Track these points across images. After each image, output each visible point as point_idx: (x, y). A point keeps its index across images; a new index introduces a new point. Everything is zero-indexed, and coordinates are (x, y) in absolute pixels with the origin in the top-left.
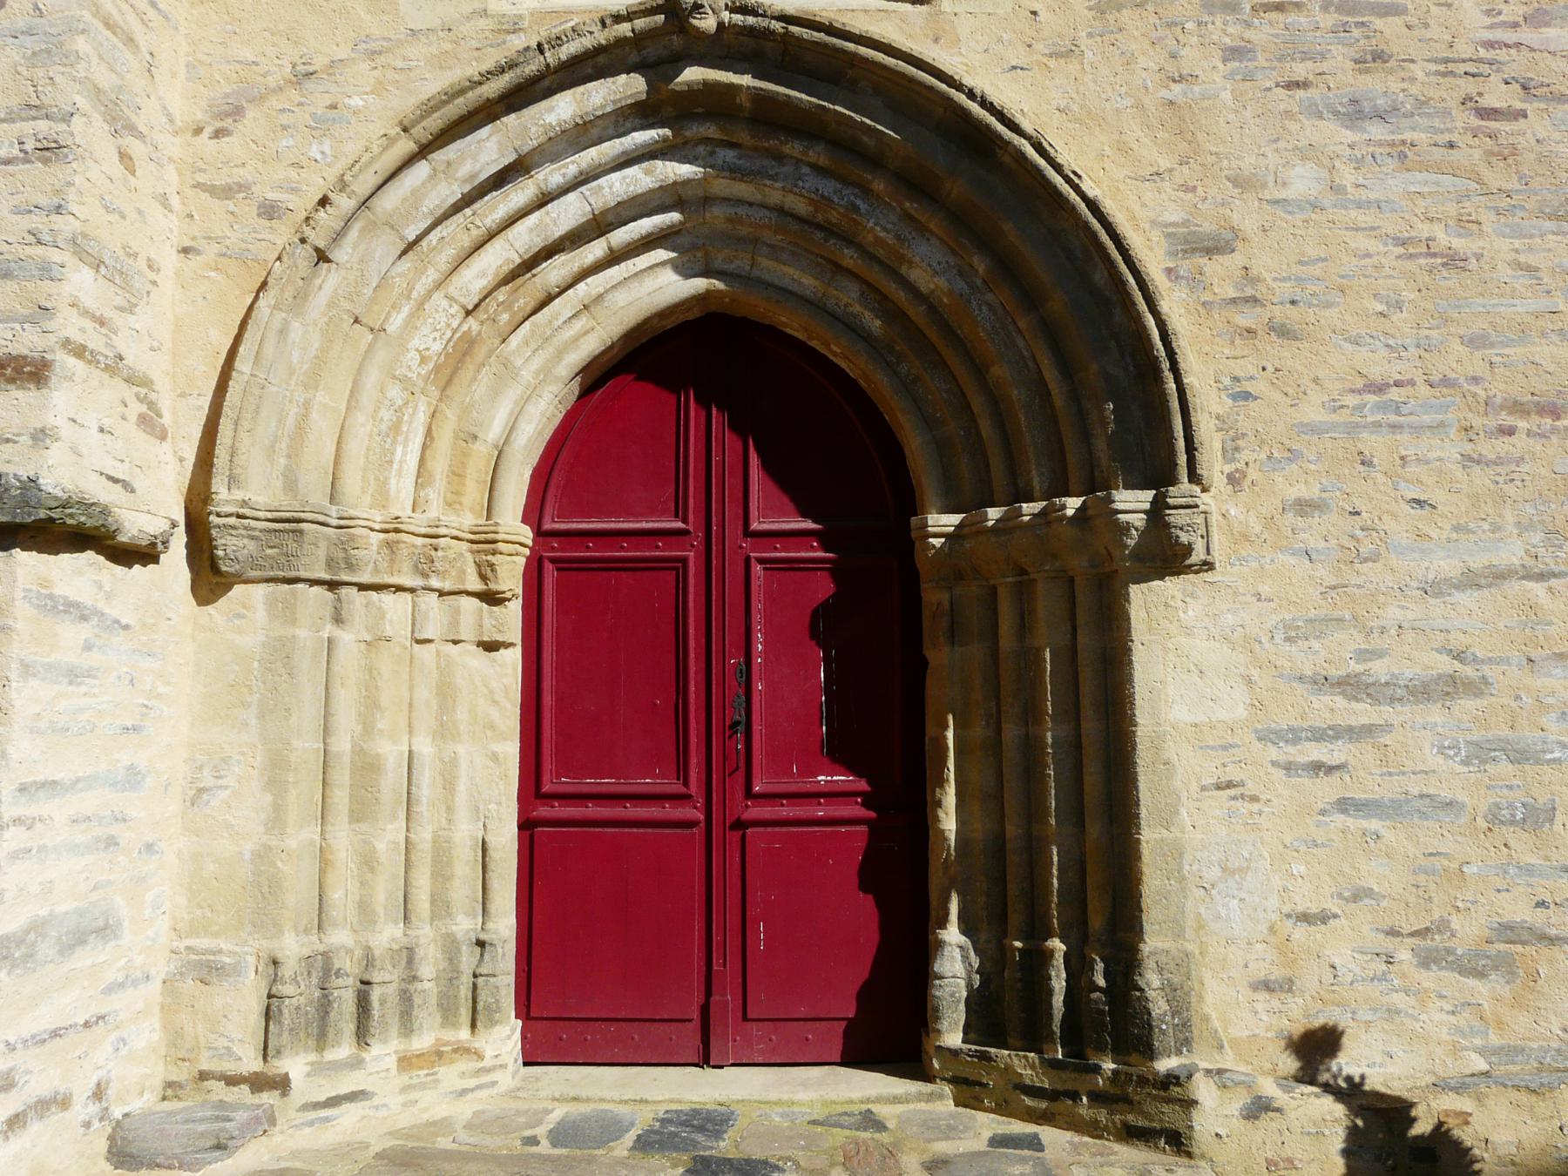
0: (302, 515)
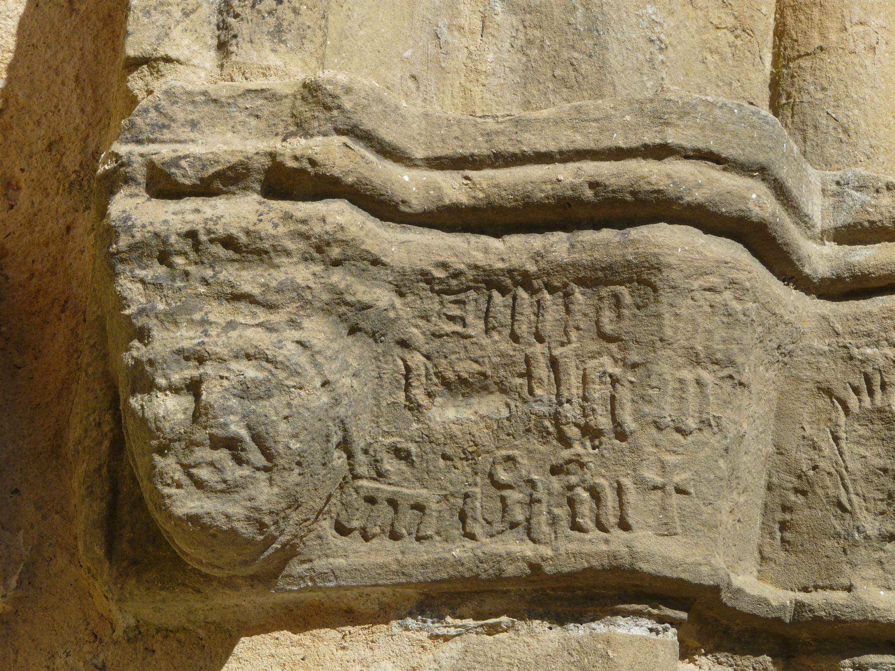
0: (654, 173)
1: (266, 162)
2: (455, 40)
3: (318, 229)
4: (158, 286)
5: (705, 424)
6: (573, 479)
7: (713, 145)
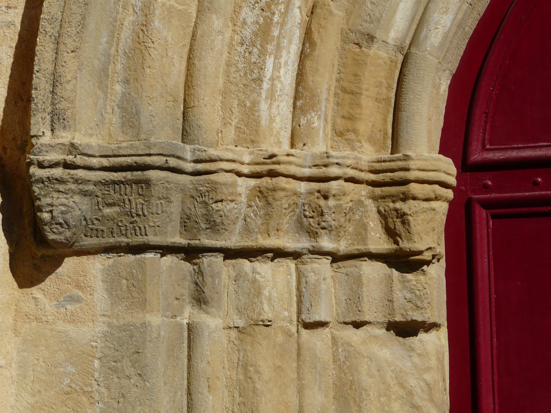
0: (148, 160)
1: (63, 161)
2: (106, 115)
3: (76, 177)
4: (42, 189)
5: (163, 212)
6: (135, 225)
7: (161, 152)
